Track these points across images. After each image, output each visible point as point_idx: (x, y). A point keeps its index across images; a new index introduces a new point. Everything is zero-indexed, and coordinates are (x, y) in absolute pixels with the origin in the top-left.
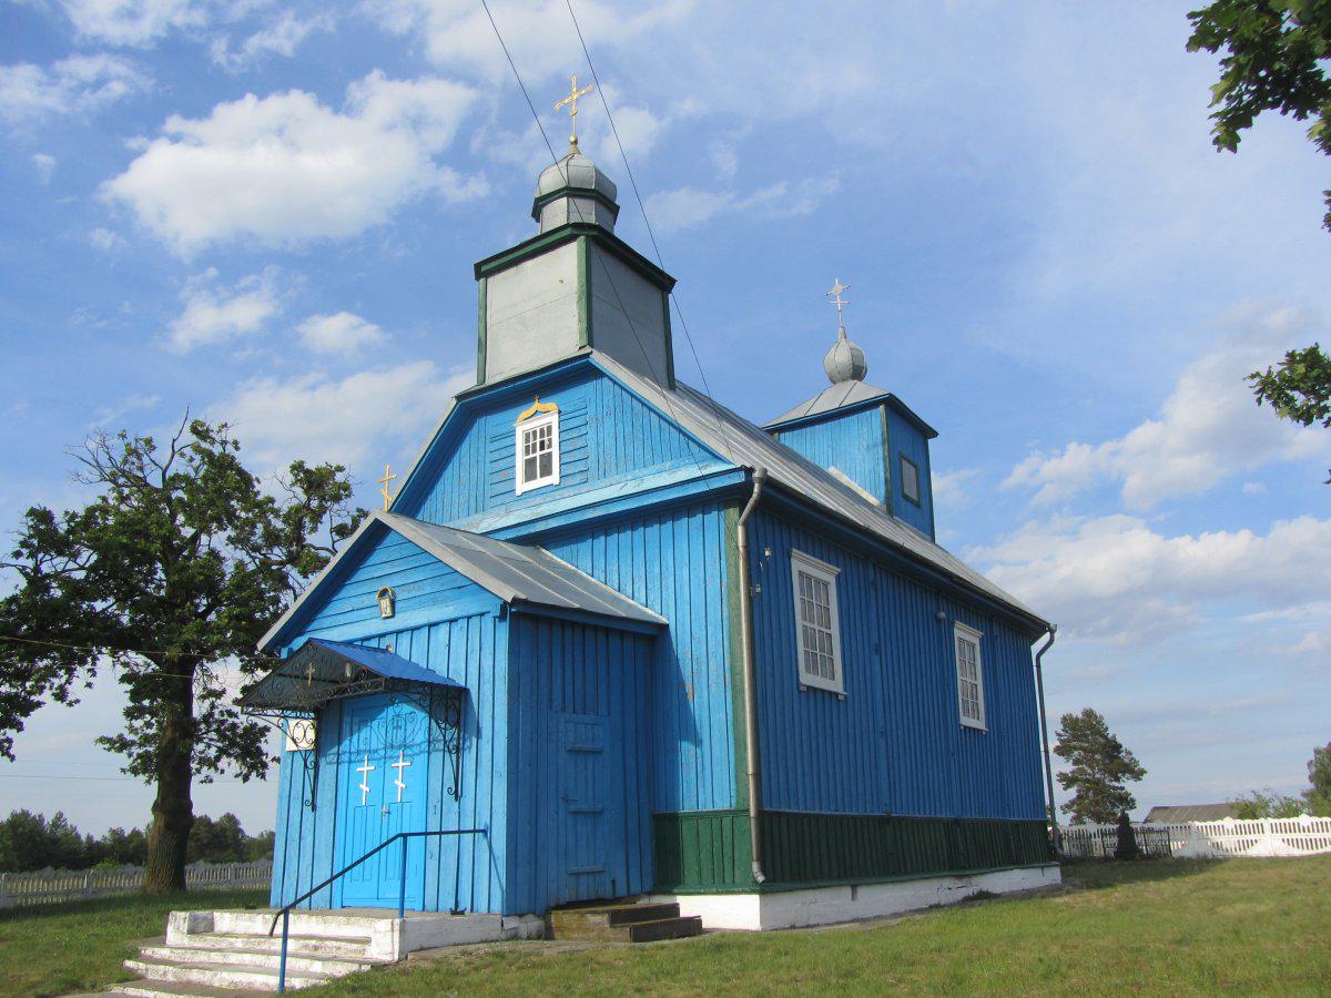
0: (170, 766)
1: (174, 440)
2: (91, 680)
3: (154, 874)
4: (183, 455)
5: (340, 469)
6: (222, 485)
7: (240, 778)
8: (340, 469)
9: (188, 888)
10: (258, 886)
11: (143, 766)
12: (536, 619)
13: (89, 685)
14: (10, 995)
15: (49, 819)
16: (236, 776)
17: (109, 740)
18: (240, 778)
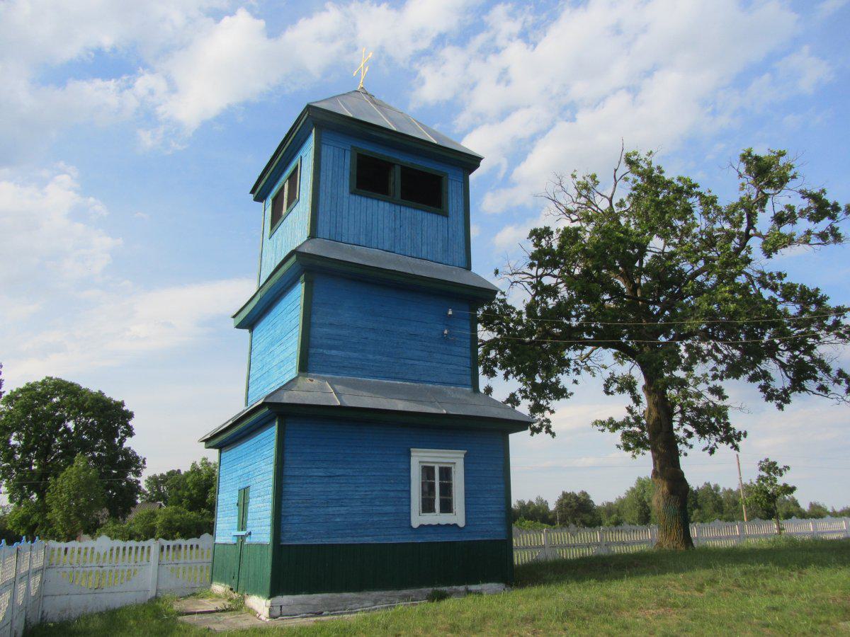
0: (657, 436)
1: (616, 170)
2: (577, 377)
3: (665, 530)
4: (626, 179)
5: (782, 154)
6: (661, 197)
7: (707, 451)
8: (782, 154)
9: (696, 545)
10: (285, 599)
11: (633, 442)
12: (629, 436)
13: (575, 382)
14: (586, 634)
15: (534, 501)
16: (704, 450)
17: (603, 423)
18: (707, 451)
